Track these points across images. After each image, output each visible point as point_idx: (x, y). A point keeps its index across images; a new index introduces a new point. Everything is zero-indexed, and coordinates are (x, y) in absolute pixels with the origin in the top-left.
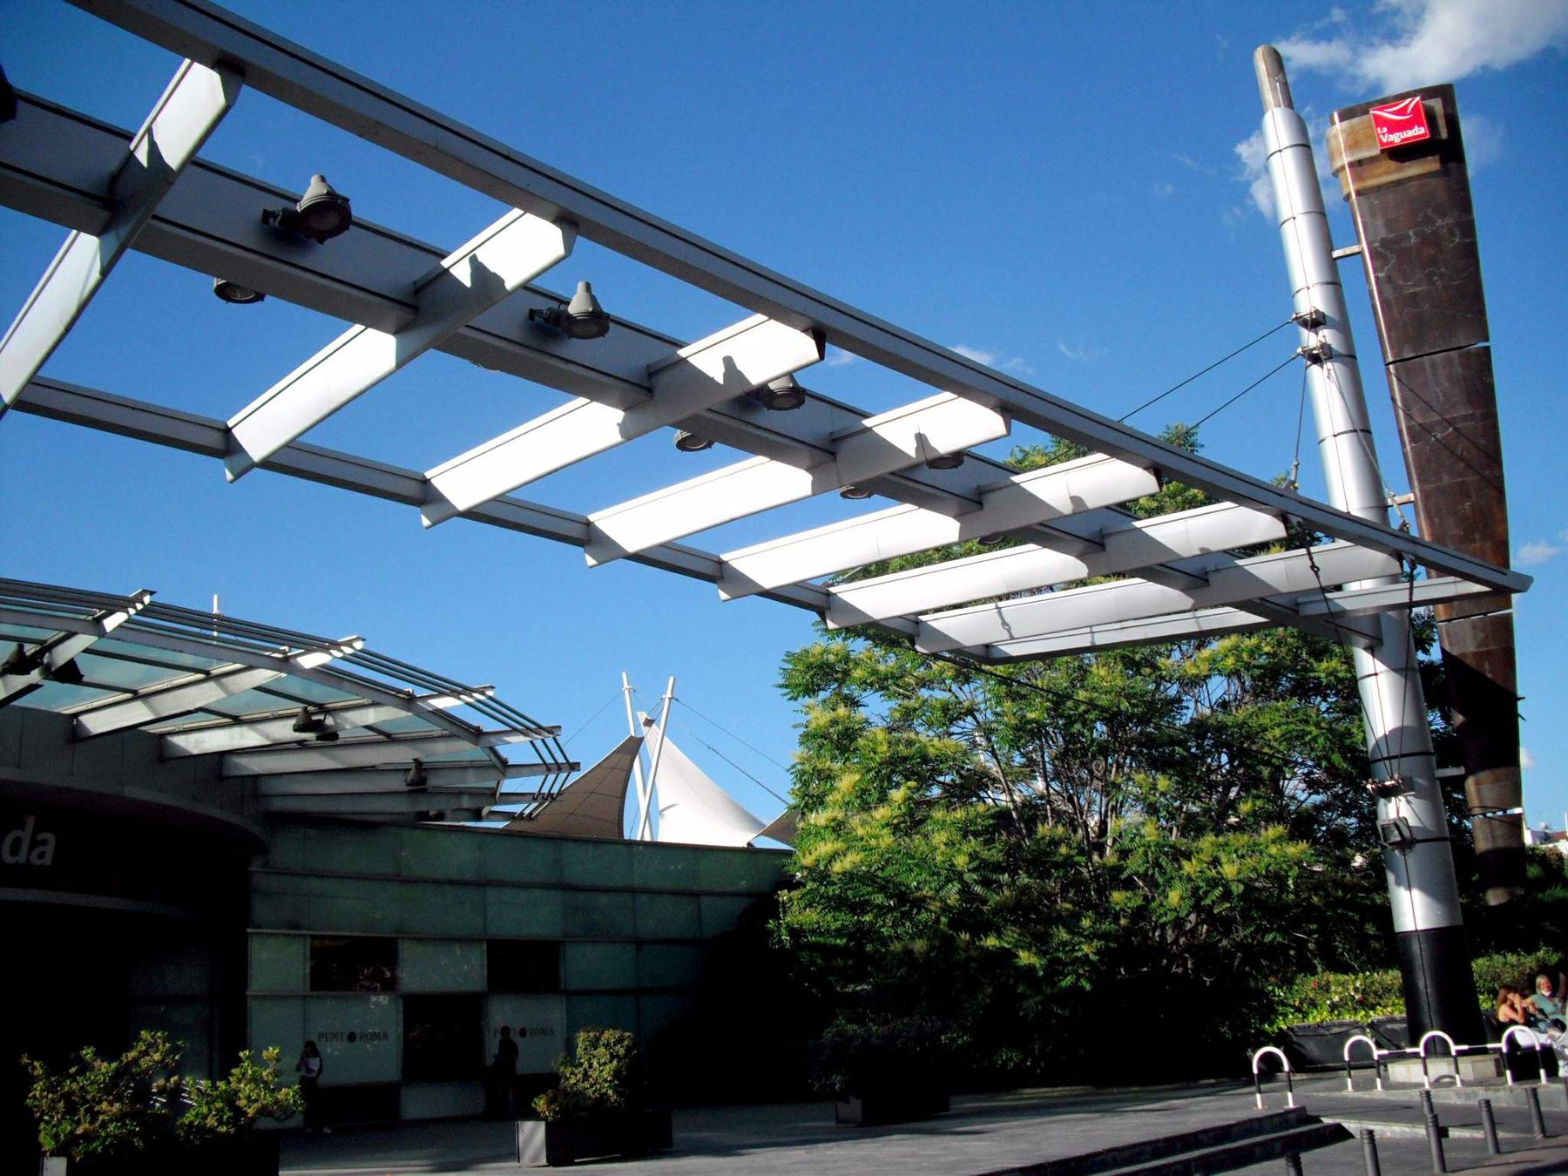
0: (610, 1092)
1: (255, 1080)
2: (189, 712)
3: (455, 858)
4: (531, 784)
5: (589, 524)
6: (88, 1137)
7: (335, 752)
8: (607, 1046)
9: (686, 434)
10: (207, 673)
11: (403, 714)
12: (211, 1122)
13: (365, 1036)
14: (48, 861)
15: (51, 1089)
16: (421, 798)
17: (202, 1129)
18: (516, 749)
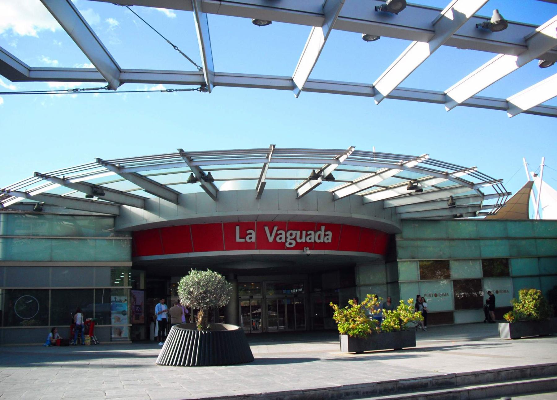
0: (533, 312)
1: (406, 310)
2: (371, 187)
3: (466, 230)
4: (493, 201)
5: (507, 102)
6: (353, 329)
8: (531, 295)
9: (543, 61)
10: (375, 173)
11: (445, 180)
12: (392, 324)
13: (440, 296)
14: (330, 241)
15: (341, 313)
16: (454, 209)
17: (388, 327)
18: (487, 189)
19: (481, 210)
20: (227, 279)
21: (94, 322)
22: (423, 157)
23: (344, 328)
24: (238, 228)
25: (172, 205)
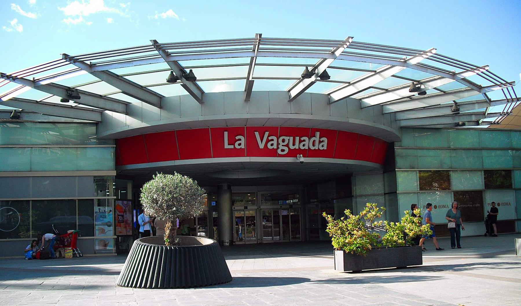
3: (467, 140)
6: (350, 244)
7: (424, 100)
11: (452, 80)
12: (395, 238)
14: (325, 148)
15: (336, 225)
18: (496, 94)
19: (485, 118)
20: (199, 184)
21: (76, 235)
22: (430, 51)
23: (339, 242)
24: (226, 134)
25: (155, 110)
